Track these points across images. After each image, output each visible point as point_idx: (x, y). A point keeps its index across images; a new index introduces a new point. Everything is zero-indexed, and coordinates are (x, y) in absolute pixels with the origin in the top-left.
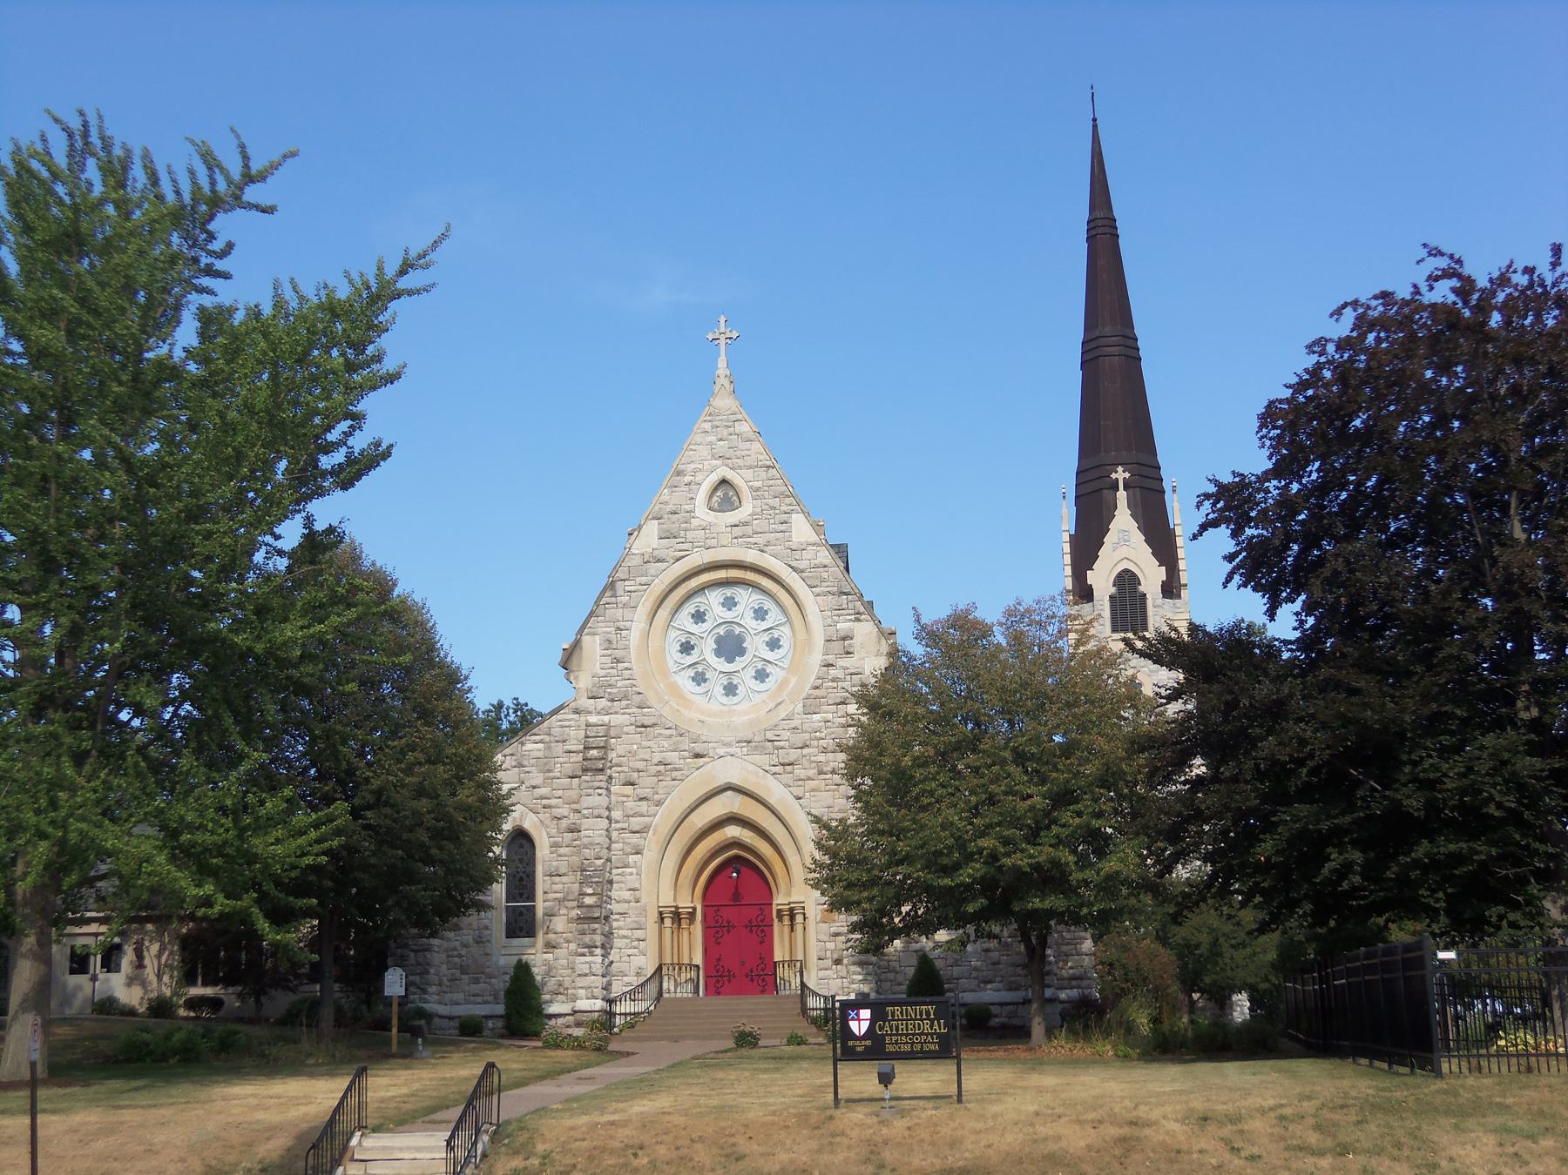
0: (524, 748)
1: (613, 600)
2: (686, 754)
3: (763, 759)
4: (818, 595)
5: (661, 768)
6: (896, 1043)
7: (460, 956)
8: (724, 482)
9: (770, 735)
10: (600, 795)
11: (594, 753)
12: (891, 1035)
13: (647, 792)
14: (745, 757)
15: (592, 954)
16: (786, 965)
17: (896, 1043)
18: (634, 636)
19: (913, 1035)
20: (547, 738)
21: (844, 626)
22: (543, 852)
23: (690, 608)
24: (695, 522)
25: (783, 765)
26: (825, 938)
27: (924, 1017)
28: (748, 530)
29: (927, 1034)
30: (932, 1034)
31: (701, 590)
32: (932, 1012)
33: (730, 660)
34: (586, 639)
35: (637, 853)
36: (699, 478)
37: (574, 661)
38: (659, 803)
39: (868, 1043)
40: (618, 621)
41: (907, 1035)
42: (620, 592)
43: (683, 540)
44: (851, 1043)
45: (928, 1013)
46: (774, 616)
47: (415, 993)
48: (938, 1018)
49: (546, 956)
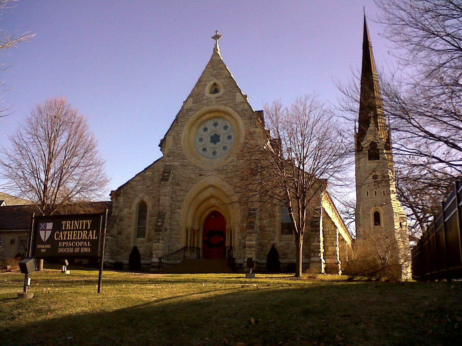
1: (177, 124)
2: (197, 175)
3: (223, 176)
4: (244, 120)
5: (189, 180)
7: (121, 243)
9: (225, 168)
10: (167, 188)
11: (166, 174)
12: (63, 241)
13: (184, 188)
14: (217, 176)
15: (159, 242)
16: (188, 249)
18: (183, 136)
19: (76, 241)
20: (152, 170)
21: (252, 129)
22: (149, 208)
23: (203, 127)
24: (204, 97)
26: (241, 239)
27: (84, 228)
29: (84, 241)
30: (87, 241)
31: (205, 121)
32: (89, 225)
33: (215, 143)
34: (167, 137)
38: (188, 192)
39: (48, 246)
40: (178, 131)
42: (179, 122)
43: (200, 104)
44: (39, 246)
46: (220, 122)
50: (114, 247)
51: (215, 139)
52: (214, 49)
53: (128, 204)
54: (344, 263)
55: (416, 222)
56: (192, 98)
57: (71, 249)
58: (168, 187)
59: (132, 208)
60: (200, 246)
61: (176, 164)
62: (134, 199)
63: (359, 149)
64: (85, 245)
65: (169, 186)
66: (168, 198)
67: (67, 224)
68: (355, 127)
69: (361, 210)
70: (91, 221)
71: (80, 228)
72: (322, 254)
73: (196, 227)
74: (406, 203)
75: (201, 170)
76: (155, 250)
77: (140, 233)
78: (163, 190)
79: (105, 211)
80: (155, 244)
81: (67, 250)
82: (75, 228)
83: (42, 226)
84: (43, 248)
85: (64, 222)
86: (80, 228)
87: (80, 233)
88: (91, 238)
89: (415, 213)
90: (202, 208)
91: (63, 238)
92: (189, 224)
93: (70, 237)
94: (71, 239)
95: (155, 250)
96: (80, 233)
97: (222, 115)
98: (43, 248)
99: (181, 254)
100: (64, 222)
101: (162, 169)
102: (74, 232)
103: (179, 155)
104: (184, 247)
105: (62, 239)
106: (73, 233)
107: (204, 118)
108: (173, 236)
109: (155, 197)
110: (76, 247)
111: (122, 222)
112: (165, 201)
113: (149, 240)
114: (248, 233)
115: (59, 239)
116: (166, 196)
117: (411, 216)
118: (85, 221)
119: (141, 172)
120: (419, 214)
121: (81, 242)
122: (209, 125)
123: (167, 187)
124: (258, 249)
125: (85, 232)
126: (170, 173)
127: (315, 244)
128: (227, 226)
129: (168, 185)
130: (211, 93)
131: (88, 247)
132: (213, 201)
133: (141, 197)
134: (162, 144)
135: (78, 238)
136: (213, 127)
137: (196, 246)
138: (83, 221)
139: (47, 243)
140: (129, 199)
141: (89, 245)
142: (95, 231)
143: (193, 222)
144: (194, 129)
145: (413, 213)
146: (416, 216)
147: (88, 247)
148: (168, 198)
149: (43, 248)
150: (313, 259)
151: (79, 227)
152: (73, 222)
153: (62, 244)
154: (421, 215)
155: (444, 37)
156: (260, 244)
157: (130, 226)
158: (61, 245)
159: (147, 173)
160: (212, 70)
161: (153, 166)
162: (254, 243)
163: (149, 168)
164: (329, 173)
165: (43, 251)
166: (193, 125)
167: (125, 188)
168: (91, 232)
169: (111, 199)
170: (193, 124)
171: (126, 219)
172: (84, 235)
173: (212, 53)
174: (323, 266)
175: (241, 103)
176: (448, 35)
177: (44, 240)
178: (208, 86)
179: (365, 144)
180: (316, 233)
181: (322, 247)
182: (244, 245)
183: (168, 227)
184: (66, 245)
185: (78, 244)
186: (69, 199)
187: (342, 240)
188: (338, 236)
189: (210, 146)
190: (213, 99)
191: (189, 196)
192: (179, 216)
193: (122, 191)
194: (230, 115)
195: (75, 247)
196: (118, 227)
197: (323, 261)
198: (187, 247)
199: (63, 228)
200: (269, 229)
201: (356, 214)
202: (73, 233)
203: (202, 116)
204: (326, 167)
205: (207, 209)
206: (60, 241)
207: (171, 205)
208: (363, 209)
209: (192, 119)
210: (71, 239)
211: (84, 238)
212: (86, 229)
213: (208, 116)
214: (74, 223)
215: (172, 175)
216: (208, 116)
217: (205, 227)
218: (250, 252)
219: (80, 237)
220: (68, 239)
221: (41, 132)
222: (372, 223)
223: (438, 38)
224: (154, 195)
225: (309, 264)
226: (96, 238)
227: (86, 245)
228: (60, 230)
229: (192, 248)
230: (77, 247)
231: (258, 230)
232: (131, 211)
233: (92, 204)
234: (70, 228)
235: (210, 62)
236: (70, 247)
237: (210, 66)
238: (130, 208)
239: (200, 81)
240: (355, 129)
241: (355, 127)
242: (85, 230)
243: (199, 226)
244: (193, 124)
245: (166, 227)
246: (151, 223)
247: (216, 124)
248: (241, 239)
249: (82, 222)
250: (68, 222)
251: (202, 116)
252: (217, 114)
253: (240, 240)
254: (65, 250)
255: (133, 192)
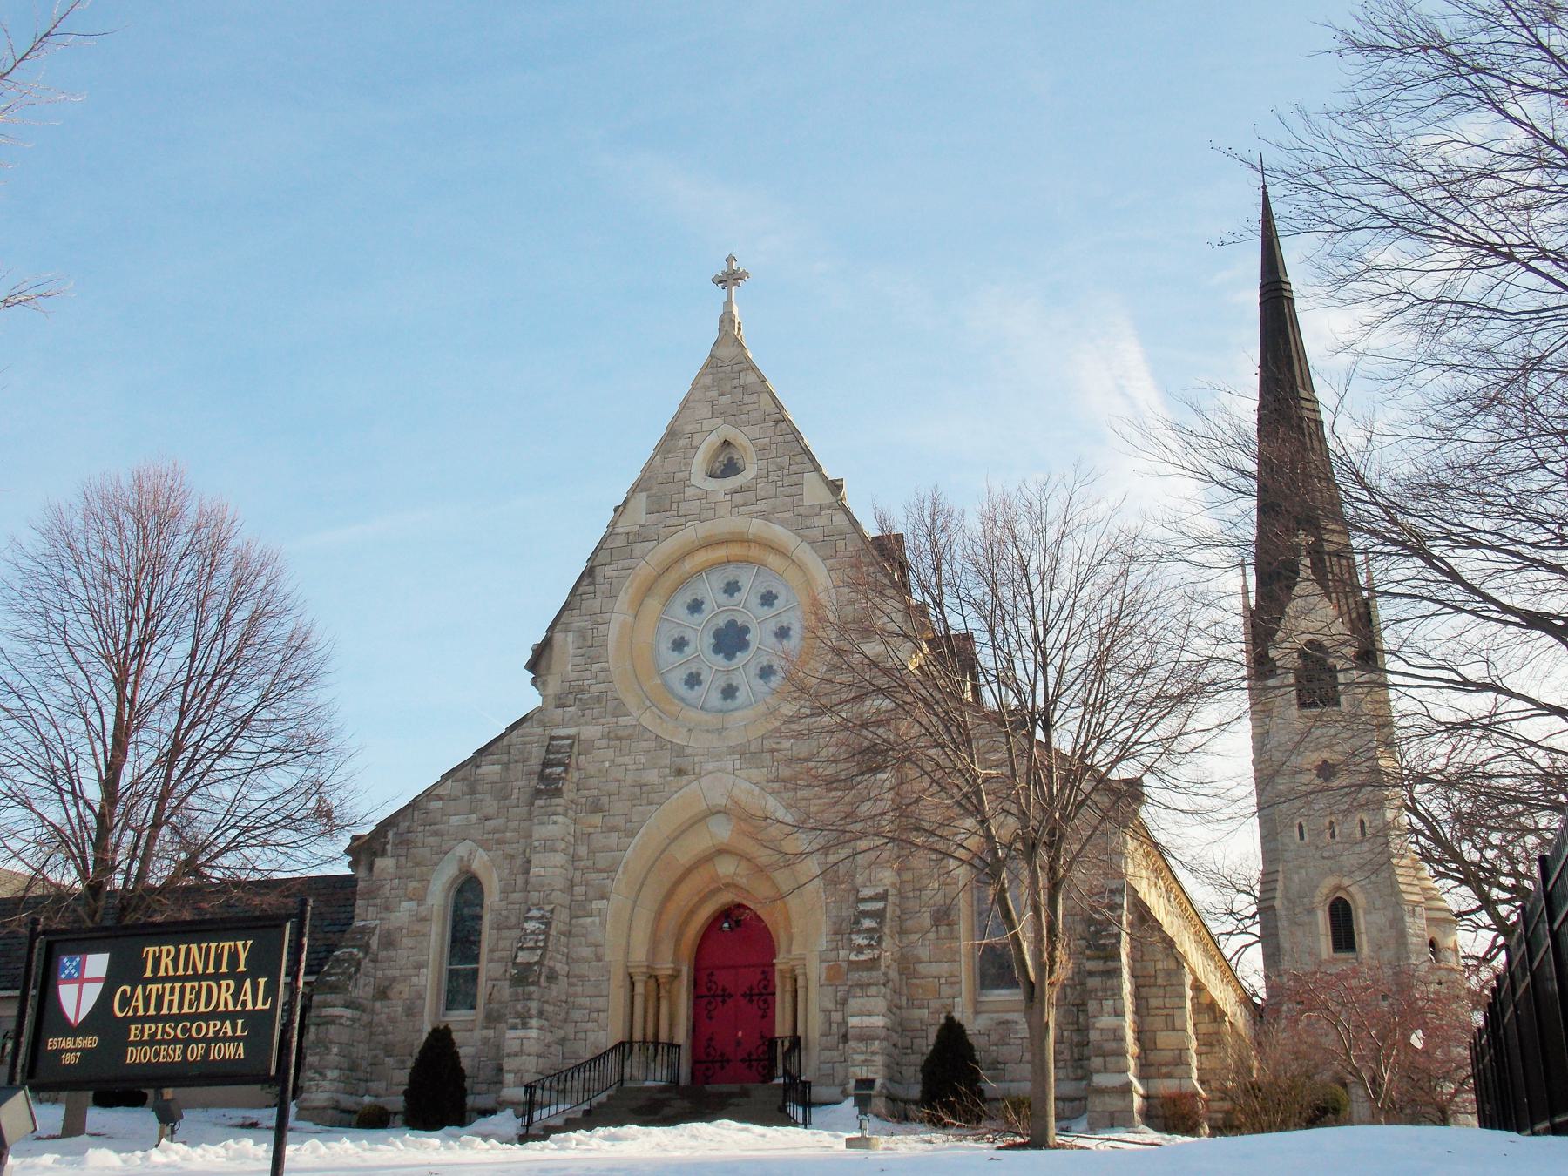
0: (479, 771)
1: (591, 588)
3: (758, 774)
6: (152, 1041)
7: (385, 1033)
8: (726, 443)
10: (555, 823)
13: (620, 821)
14: (737, 772)
15: (525, 1026)
16: (636, 1047)
17: (152, 1041)
19: (193, 1018)
20: (505, 758)
23: (686, 597)
24: (690, 492)
25: (783, 781)
26: (831, 1006)
27: (224, 969)
28: (752, 495)
30: (232, 1016)
32: (243, 956)
34: (558, 637)
35: (602, 898)
36: (696, 440)
37: (543, 663)
38: (632, 834)
39: (90, 1042)
41: (179, 1018)
42: (599, 579)
44: (53, 1043)
45: (234, 956)
46: (747, 578)
47: (312, 1079)
48: (253, 973)
49: (485, 1032)
50: (361, 1045)
51: (731, 640)
52: (721, 321)
53: (413, 884)
54: (1218, 1094)
55: (1495, 938)
56: (644, 495)
57: (174, 1051)
58: (560, 819)
59: (430, 901)
60: (682, 1037)
61: (589, 731)
62: (436, 864)
63: (1261, 666)
64: (225, 1033)
65: (565, 815)
66: (559, 859)
67: (161, 956)
68: (1245, 586)
69: (1279, 894)
70: (250, 942)
71: (211, 970)
72: (1132, 1063)
73: (665, 968)
74: (1452, 870)
75: (680, 751)
76: (508, 1055)
77: (460, 989)
78: (540, 832)
79: (304, 903)
80: (511, 1034)
81: (157, 1054)
82: (190, 972)
83: (68, 964)
84: (71, 1051)
85: (151, 949)
86: (211, 970)
87: (209, 988)
88: (250, 1006)
89: (1488, 904)
90: (685, 894)
91: (146, 1008)
92: (640, 955)
93: (171, 1002)
94: (175, 1011)
95: (508, 1055)
96: (209, 988)
97: (754, 552)
98: (69, 1050)
99: (611, 1066)
100: (150, 951)
101: (537, 755)
102: (188, 985)
103: (599, 700)
104: (622, 1043)
105: (141, 1012)
106: (183, 989)
107: (688, 565)
108: (581, 1001)
109: (512, 857)
110: (191, 1040)
111: (392, 953)
112: (549, 868)
113: (492, 1019)
114: (857, 985)
115: (130, 1014)
116: (553, 850)
117: (1472, 917)
118: (227, 944)
119: (463, 765)
120: (1503, 910)
121: (212, 1023)
122: (710, 590)
123: (555, 818)
124: (895, 1046)
125: (228, 986)
126: (567, 767)
127: (1106, 1021)
128: (781, 962)
129: (559, 809)
130: (712, 475)
131: (239, 1039)
132: (726, 868)
133: (462, 859)
134: (538, 662)
135: (202, 1009)
136: (723, 598)
137: (663, 1037)
138: (221, 944)
139: (85, 1028)
140: (417, 864)
141: (239, 1033)
142: (262, 981)
143: (655, 943)
144: (653, 604)
145: (1479, 903)
146: (1490, 915)
147: (239, 1039)
148: (559, 859)
149: (71, 1051)
150: (1100, 1080)
151: (206, 967)
152: (183, 947)
153: (142, 1031)
154: (1512, 912)
155: (1534, 263)
156: (901, 1025)
157: (419, 966)
158: (136, 1036)
159: (485, 769)
160: (714, 393)
161: (505, 742)
162: (879, 1021)
163: (493, 749)
164: (1142, 759)
165: (69, 1059)
166: (648, 590)
167: (404, 826)
168: (248, 983)
169: (350, 865)
170: (649, 589)
171: (407, 942)
172: (223, 996)
173: (716, 335)
174: (1137, 1102)
175: (821, 507)
176: (1544, 254)
177: (72, 1020)
178: (702, 448)
179: (1283, 653)
180: (1109, 983)
181: (1130, 1036)
182: (843, 1030)
183: (561, 968)
184: (156, 1031)
185: (199, 1029)
186: (197, 872)
187: (1211, 1010)
188: (1189, 993)
189: (713, 666)
190: (721, 496)
191: (636, 853)
192: (603, 925)
193: (390, 835)
194: (780, 552)
195: (187, 1042)
196: (376, 969)
197: (1138, 1087)
198: (631, 1043)
199: (145, 972)
200: (934, 969)
201: (1266, 911)
202: (183, 989)
203: (681, 558)
204: (1128, 739)
205: (703, 900)
206: (136, 1019)
207: (572, 884)
208: (1286, 889)
209: (644, 570)
210: (175, 1011)
211: (221, 1008)
212: (233, 974)
213: (702, 557)
214: (188, 951)
215: (574, 775)
216: (702, 557)
217: (698, 968)
218: (863, 1057)
219: (208, 1004)
220: (165, 1011)
221: (82, 630)
222: (1325, 944)
223: (1512, 266)
224: (509, 849)
225: (1086, 1099)
226: (268, 1006)
227: (230, 1034)
228: (136, 978)
229: (656, 1046)
230: (197, 1041)
231: (893, 974)
232: (423, 911)
233: (268, 885)
234: (171, 973)
235: (707, 366)
236: (168, 1043)
237: (708, 380)
238: (420, 899)
239: (672, 433)
240: (1245, 592)
241: (1245, 586)
242: (225, 976)
243: (673, 962)
244: (649, 589)
245: (552, 969)
246: (497, 955)
247: (732, 588)
248: (831, 1006)
249: (217, 947)
250: (165, 949)
251: (681, 558)
252: (735, 550)
253: (826, 1012)
254: (151, 1054)
255: (432, 840)
